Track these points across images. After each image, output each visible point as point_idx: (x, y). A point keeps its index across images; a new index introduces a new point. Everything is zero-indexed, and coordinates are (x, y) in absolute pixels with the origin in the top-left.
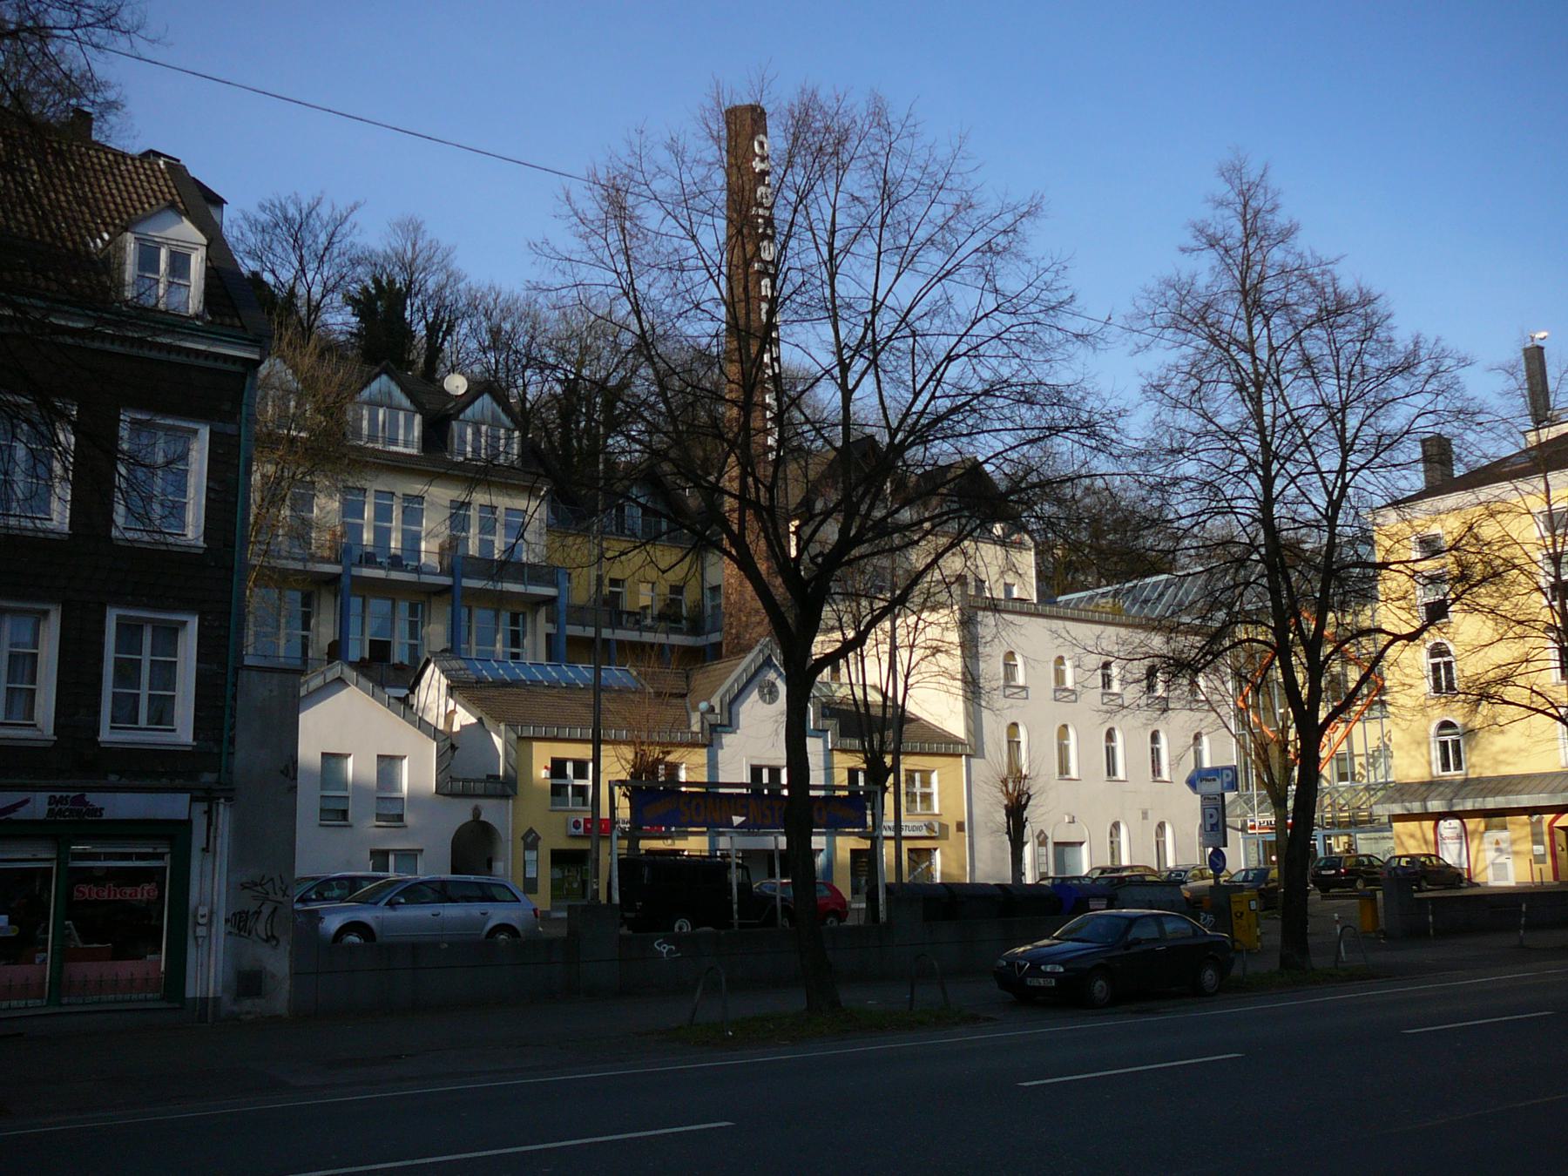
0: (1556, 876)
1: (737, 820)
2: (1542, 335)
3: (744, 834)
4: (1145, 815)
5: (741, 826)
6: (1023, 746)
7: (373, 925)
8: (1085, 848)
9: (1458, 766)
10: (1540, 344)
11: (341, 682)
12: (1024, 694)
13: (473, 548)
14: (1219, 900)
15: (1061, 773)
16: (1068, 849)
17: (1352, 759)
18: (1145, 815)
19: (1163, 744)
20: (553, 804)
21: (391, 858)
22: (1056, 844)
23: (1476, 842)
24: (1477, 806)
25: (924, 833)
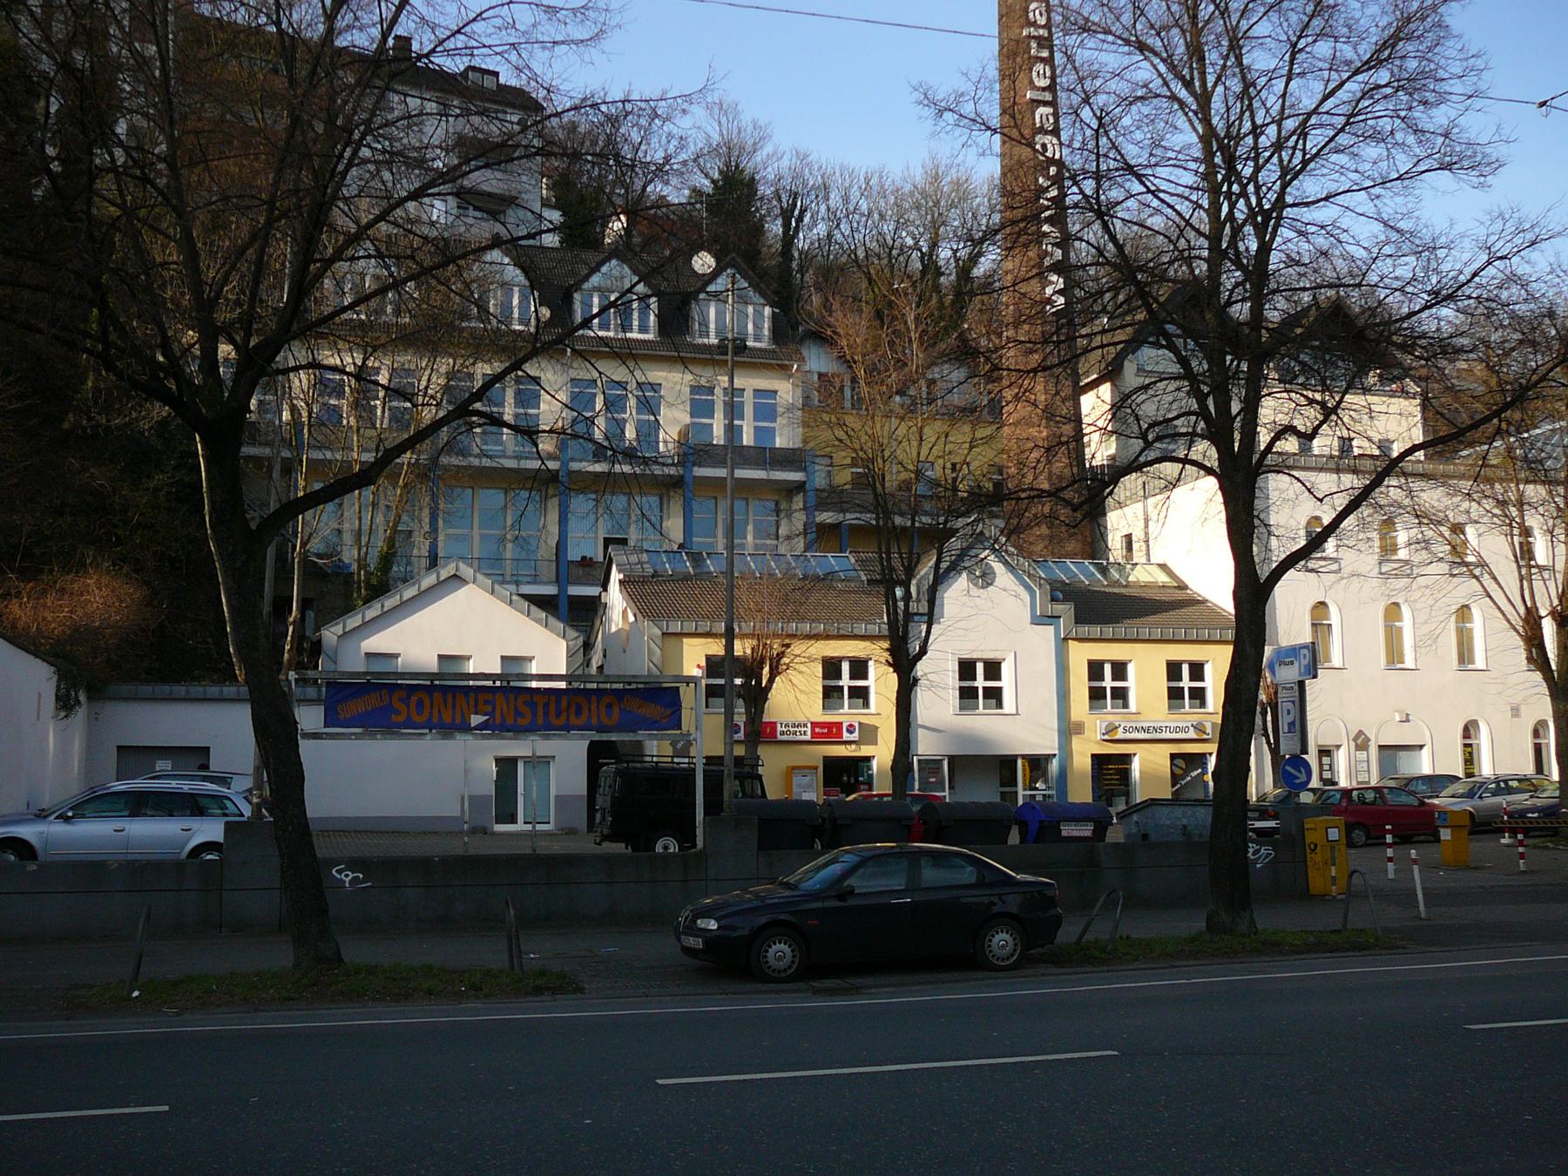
1: (476, 720)
3: (485, 737)
4: (1516, 712)
5: (481, 727)
6: (1336, 630)
7: (33, 841)
8: (1425, 752)
11: (457, 580)
12: (1335, 567)
13: (747, 439)
15: (1461, 660)
16: (1402, 754)
18: (1516, 712)
19: (1406, 624)
20: (1091, 708)
21: (520, 766)
25: (1192, 734)
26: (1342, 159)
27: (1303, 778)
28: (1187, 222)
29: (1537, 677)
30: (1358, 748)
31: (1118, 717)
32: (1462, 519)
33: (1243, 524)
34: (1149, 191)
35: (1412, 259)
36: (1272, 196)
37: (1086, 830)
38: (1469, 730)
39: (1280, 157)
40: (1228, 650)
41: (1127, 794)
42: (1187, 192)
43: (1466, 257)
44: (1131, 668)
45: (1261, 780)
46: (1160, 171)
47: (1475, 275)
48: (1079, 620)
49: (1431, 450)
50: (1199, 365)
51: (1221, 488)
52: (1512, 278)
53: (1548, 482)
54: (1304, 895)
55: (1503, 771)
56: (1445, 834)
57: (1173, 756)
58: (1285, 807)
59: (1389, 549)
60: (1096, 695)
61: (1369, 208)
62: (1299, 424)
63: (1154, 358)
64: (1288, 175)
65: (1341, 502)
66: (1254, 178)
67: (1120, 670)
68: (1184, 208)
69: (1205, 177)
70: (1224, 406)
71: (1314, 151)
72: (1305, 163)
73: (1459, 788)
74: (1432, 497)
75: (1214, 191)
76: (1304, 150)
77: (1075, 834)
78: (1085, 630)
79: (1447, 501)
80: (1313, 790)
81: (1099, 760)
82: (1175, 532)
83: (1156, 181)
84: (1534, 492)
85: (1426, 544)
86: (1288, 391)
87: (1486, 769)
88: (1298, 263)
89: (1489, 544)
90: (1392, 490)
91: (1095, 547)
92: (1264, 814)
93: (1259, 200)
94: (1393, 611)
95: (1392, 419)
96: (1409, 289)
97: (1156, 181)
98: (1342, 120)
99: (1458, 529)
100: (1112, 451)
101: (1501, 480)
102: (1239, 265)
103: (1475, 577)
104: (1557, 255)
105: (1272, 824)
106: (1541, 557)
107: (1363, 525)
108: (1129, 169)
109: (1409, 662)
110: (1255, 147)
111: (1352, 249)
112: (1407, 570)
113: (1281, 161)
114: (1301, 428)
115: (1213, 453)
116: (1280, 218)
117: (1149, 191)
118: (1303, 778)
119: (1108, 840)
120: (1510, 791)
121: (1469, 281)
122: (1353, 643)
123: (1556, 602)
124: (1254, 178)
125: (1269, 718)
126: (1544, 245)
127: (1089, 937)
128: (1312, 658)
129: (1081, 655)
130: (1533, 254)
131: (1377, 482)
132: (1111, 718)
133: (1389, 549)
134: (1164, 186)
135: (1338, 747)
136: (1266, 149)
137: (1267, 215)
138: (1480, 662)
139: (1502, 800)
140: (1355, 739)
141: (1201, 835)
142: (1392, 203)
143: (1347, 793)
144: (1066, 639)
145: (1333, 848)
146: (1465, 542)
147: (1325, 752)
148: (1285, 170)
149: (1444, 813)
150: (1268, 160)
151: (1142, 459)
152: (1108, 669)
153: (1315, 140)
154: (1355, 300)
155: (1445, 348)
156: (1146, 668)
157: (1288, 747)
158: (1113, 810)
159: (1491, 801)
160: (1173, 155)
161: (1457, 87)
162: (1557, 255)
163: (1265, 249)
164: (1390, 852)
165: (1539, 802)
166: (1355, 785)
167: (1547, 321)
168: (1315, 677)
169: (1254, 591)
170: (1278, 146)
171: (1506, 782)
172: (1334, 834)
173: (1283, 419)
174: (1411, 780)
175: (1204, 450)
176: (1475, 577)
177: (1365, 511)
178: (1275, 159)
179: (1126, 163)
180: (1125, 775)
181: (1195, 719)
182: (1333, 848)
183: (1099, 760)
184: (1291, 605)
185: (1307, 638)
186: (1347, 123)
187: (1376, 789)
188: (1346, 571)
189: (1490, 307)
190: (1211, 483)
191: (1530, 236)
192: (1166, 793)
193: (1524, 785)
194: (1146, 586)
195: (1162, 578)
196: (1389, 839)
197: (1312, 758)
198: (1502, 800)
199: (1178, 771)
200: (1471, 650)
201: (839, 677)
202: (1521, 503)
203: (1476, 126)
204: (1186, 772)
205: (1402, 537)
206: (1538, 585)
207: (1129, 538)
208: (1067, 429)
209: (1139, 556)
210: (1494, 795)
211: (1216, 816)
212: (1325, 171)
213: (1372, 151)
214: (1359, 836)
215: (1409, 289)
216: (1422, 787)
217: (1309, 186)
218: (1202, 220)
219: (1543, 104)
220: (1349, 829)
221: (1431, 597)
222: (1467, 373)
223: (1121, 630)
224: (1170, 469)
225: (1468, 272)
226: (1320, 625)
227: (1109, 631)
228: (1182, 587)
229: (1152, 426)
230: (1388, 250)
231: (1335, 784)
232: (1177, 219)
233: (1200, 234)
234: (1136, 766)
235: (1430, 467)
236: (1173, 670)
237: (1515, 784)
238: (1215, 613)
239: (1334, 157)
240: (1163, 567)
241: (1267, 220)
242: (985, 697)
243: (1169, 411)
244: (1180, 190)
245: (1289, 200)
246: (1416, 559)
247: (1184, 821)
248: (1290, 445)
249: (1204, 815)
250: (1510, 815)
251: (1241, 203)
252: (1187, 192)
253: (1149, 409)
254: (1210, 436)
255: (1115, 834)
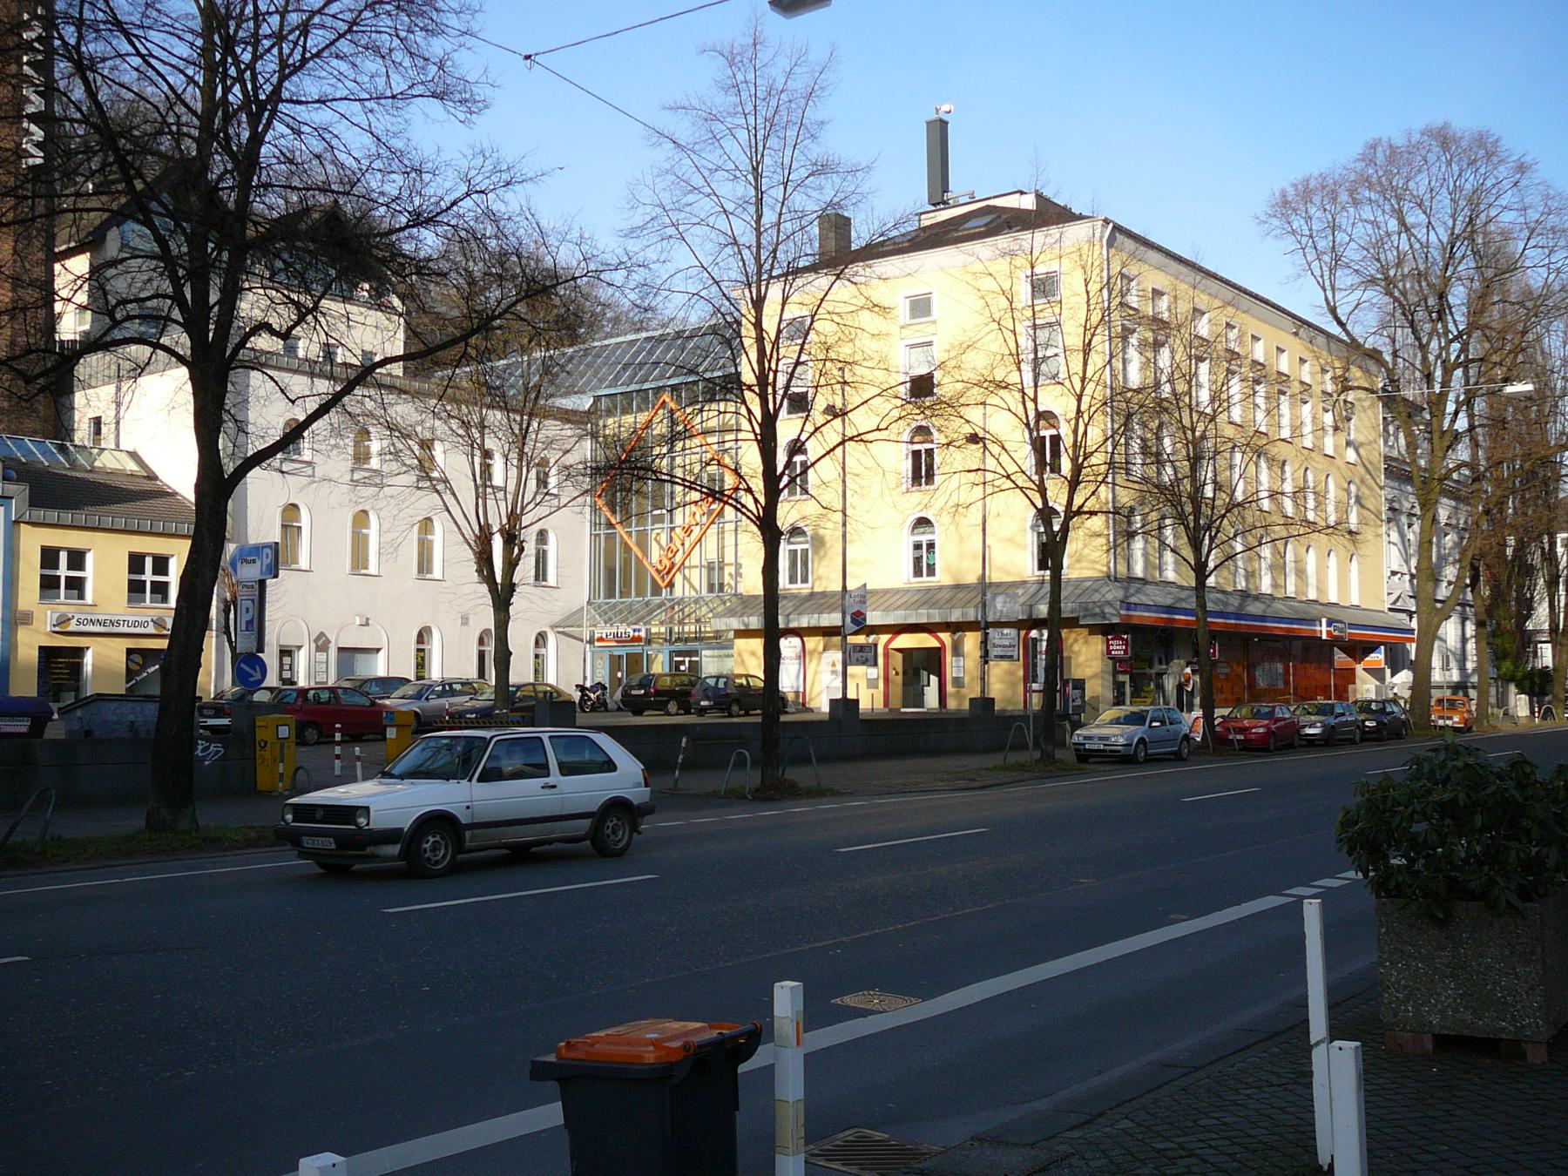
0: (886, 703)
2: (946, 108)
4: (465, 620)
8: (382, 655)
9: (805, 580)
10: (945, 117)
12: (309, 471)
14: (1023, 718)
15: (421, 570)
16: (359, 656)
17: (721, 569)
18: (465, 620)
19: (373, 532)
20: (42, 597)
22: (340, 649)
23: (814, 662)
24: (814, 623)
25: (151, 629)
26: (343, 66)
27: (258, 676)
28: (178, 97)
29: (484, 588)
30: (318, 649)
31: (72, 609)
32: (428, 435)
33: (211, 415)
34: (138, 54)
35: (399, 179)
36: (268, 88)
37: (22, 726)
38: (423, 636)
39: (281, 49)
40: (186, 545)
41: (77, 689)
42: (182, 65)
43: (448, 185)
44: (89, 558)
45: (214, 674)
46: (152, 34)
47: (454, 203)
48: (34, 502)
49: (411, 364)
50: (179, 246)
51: (191, 378)
52: (490, 215)
53: (506, 408)
54: (250, 791)
55: (450, 675)
56: (391, 733)
57: (130, 651)
58: (241, 707)
59: (361, 457)
60: (49, 584)
61: (361, 119)
62: (275, 322)
63: (137, 234)
64: (287, 70)
65: (312, 405)
66: (251, 66)
67: (77, 559)
68: (177, 80)
69: (206, 51)
70: (201, 294)
71: (314, 51)
72: (304, 61)
73: (409, 690)
74: (403, 411)
75: (211, 69)
76: (304, 47)
77: (9, 729)
78: (40, 514)
79: (416, 417)
80: (271, 689)
81: (46, 653)
82: (143, 420)
83: (148, 45)
84: (495, 417)
85: (396, 454)
86: (264, 288)
87: (435, 673)
88: (291, 161)
89: (451, 460)
90: (362, 400)
91: (60, 428)
92: (219, 711)
93: (255, 89)
94: (361, 518)
95: (370, 330)
96: (394, 205)
97: (148, 45)
98: (343, 27)
99: (427, 445)
100: (87, 327)
101: (467, 403)
102: (227, 149)
103: (437, 491)
104: (528, 199)
105: (226, 721)
106: (498, 480)
107: (337, 432)
108: (118, 25)
109: (373, 568)
110: (255, 35)
111: (342, 157)
112: (377, 480)
113: (281, 53)
114: (276, 327)
115: (185, 339)
116: (274, 112)
117: (138, 54)
118: (258, 676)
119: (46, 736)
120: (453, 693)
121: (449, 208)
122: (321, 545)
123: (505, 521)
124: (251, 66)
125: (232, 616)
126: (517, 187)
127: (16, 838)
128: (275, 558)
129: (33, 541)
130: (509, 195)
131: (348, 390)
132: (63, 609)
133: (361, 457)
134: (157, 52)
135: (299, 647)
136: (266, 37)
137: (262, 106)
138: (437, 573)
139: (445, 702)
140: (316, 641)
141: (148, 732)
142: (383, 121)
143: (303, 692)
144: (17, 522)
145: (282, 746)
146: (432, 458)
147: (286, 652)
148: (283, 63)
149: (391, 712)
150: (269, 50)
151: (108, 339)
152: (149, 562)
153: (316, 39)
154: (348, 207)
155: (422, 267)
156: (106, 559)
157: (245, 644)
158: (54, 706)
159: (435, 702)
160: (169, 21)
161: (452, 21)
162: (528, 199)
163: (257, 140)
164: (338, 750)
165: (478, 704)
166: (313, 685)
167: (514, 258)
168: (276, 576)
169: (218, 485)
170: (279, 37)
171: (450, 685)
172: (284, 732)
173: (258, 314)
174: (365, 681)
175: (179, 339)
176: (437, 491)
177: (333, 416)
178: (275, 51)
179: (115, 17)
180: (77, 668)
181: (155, 614)
182: (282, 746)
183: (46, 653)
184: (261, 503)
185: (275, 536)
186: (350, 30)
187: (332, 690)
188: (319, 472)
189: (468, 240)
190: (183, 372)
191: (506, 176)
192: (120, 688)
193: (467, 688)
194: (112, 473)
195: (131, 466)
196: (338, 737)
197: (270, 657)
198: (445, 702)
199: (133, 667)
200: (430, 561)
201: (57, 568)
202: (482, 427)
203: (468, 64)
204: (144, 667)
205: (375, 446)
206: (491, 503)
207: (97, 422)
208: (30, 295)
209: (108, 441)
210: (439, 697)
211: (163, 711)
212: (324, 74)
213: (372, 65)
214: (312, 734)
215: (394, 205)
216: (374, 689)
217: (306, 85)
218: (194, 96)
219: (528, 57)
220: (300, 729)
221: (398, 507)
222: (444, 298)
223: (81, 517)
224: (140, 352)
225: (448, 199)
226: (290, 525)
227: (67, 517)
228: (152, 477)
229: (119, 303)
230: (377, 164)
231: (294, 683)
232: (169, 93)
233: (194, 113)
234: (88, 659)
235: (406, 384)
236: (136, 562)
237: (458, 687)
238: (182, 503)
239: (334, 62)
240: (134, 455)
241: (263, 109)
242: (67, 588)
243: (142, 290)
244: (174, 61)
245: (285, 95)
246: (385, 468)
247: (132, 718)
248: (263, 342)
249: (152, 709)
250: (452, 715)
251: (237, 89)
252: (182, 65)
253: (119, 285)
254: (187, 326)
255: (56, 730)
